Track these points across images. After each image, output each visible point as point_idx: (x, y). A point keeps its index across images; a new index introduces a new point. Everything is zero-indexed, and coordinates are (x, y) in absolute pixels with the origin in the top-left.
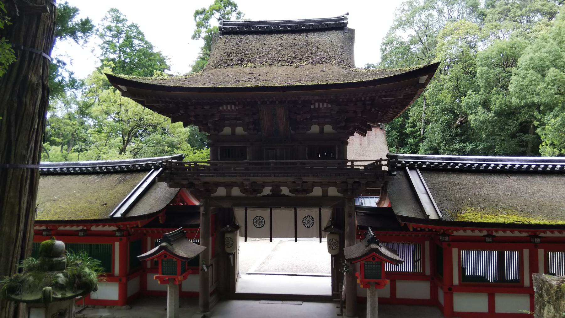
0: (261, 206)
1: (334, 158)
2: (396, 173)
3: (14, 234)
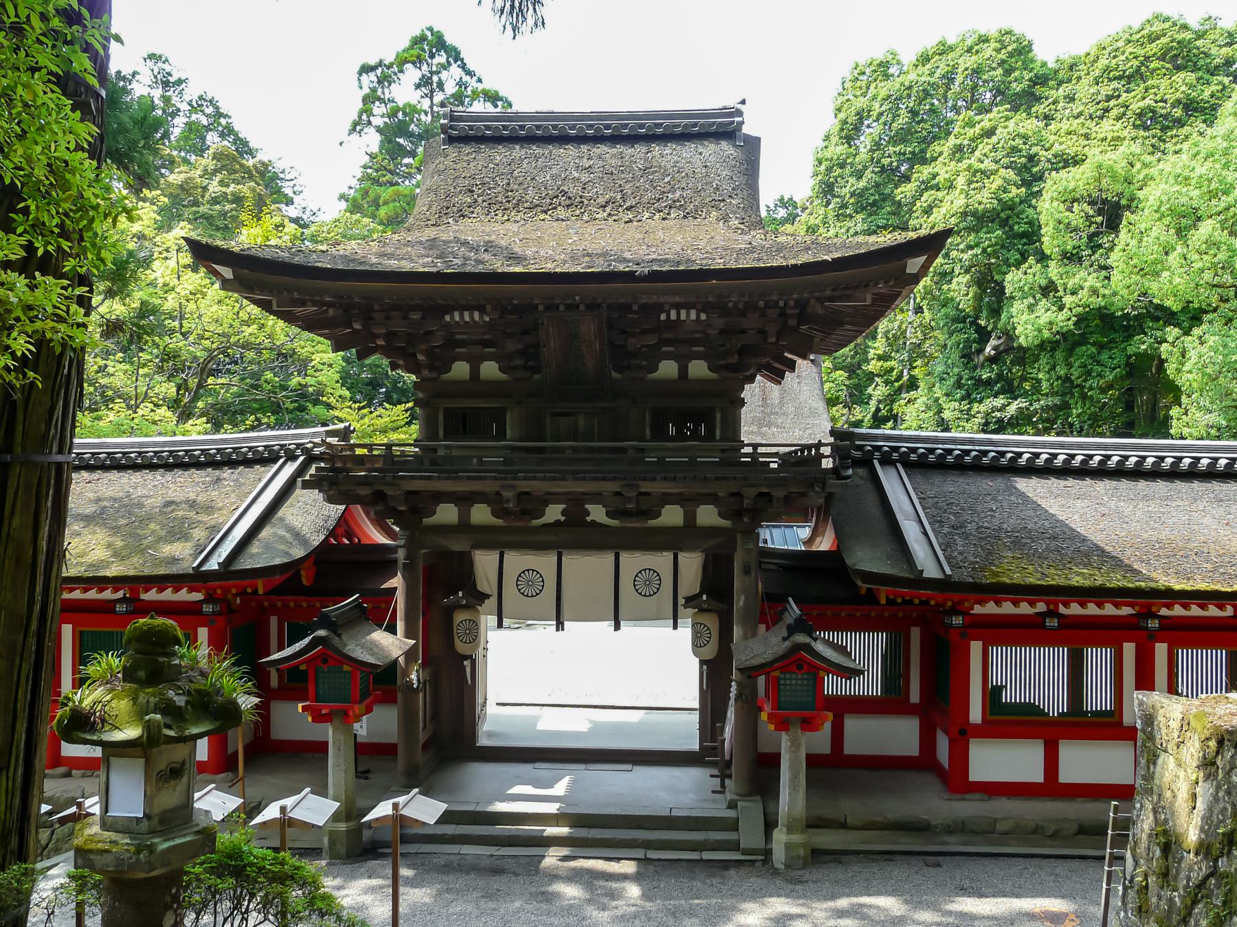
0: (539, 547)
1: (710, 436)
2: (850, 472)
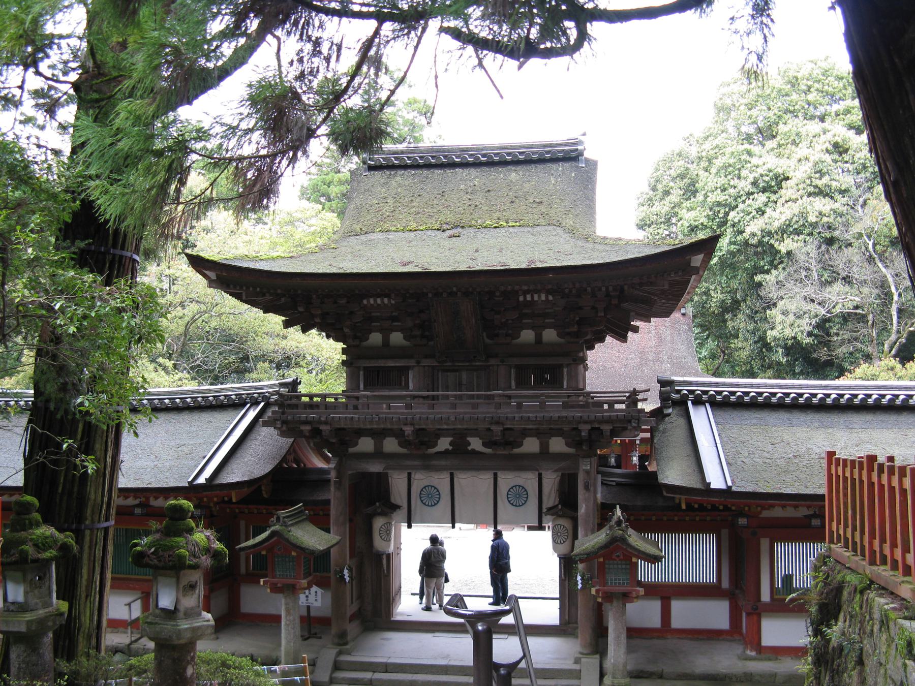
3: (99, 499)
